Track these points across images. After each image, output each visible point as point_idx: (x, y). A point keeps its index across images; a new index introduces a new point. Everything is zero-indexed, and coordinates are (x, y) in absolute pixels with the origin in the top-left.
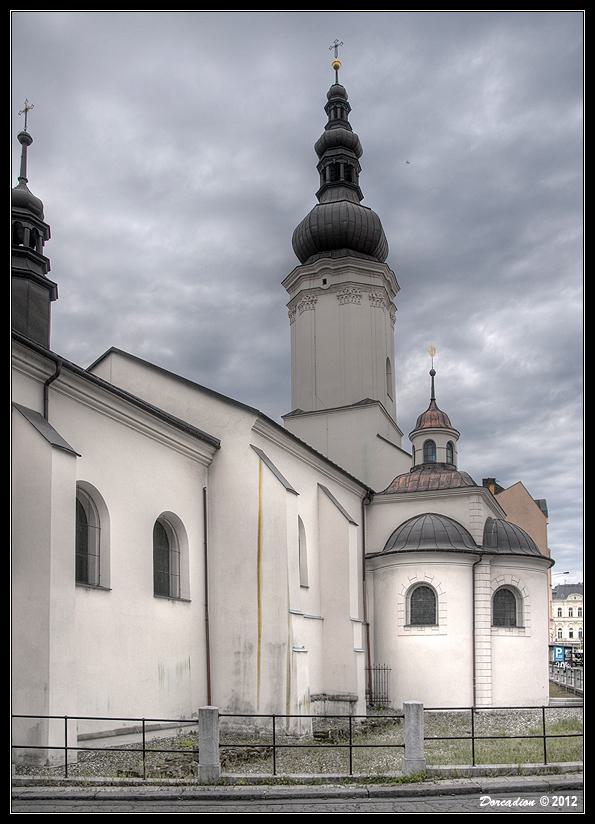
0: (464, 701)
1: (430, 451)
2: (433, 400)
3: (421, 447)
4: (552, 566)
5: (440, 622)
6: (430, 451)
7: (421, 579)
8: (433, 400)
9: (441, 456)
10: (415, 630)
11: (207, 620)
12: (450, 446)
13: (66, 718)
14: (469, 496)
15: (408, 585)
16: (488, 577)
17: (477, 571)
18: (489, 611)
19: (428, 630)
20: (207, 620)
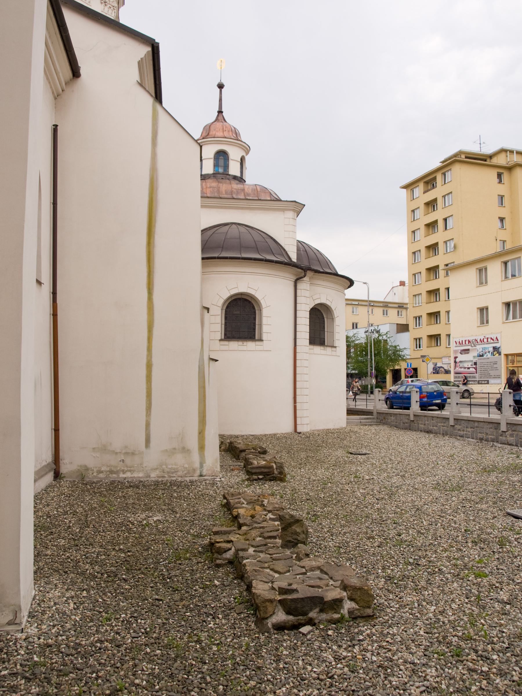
0: (285, 427)
1: (221, 162)
2: (220, 112)
3: (212, 155)
4: (349, 287)
5: (265, 337)
6: (221, 162)
7: (242, 289)
8: (220, 112)
9: (234, 169)
10: (234, 345)
11: (55, 315)
12: (242, 160)
13: (489, 393)
14: (283, 210)
15: (226, 295)
16: (307, 294)
17: (299, 286)
18: (307, 329)
19: (250, 345)
20: (55, 315)
